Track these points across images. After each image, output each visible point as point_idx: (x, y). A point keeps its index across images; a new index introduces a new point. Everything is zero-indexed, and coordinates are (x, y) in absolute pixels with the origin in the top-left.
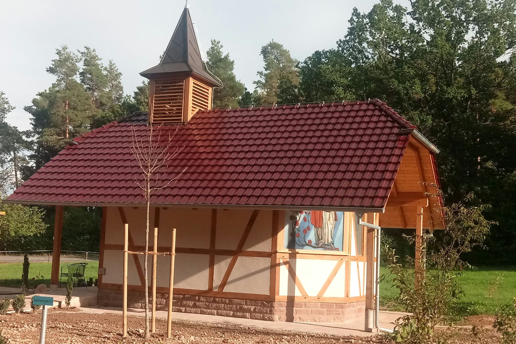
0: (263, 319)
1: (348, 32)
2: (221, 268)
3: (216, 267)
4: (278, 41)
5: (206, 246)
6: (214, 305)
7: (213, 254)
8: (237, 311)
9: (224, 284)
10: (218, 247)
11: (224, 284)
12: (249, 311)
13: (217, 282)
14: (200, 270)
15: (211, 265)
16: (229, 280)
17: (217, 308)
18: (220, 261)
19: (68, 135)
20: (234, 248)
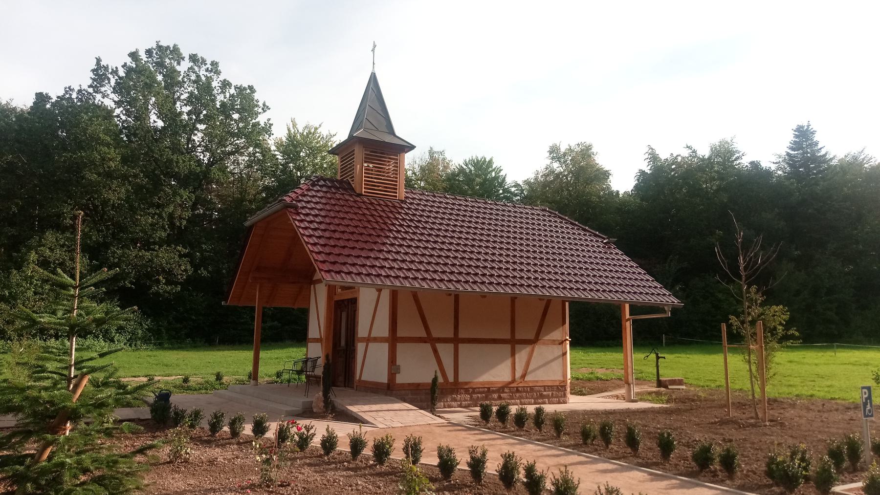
0: (559, 403)
1: (618, 192)
2: (522, 355)
3: (517, 356)
4: (814, 127)
5: (508, 336)
6: (518, 395)
7: (514, 343)
8: (537, 398)
9: (523, 376)
10: (518, 336)
11: (523, 376)
12: (548, 397)
13: (518, 374)
14: (502, 361)
15: (513, 354)
16: (531, 368)
17: (521, 398)
18: (520, 350)
19: (72, 386)
20: (531, 336)
